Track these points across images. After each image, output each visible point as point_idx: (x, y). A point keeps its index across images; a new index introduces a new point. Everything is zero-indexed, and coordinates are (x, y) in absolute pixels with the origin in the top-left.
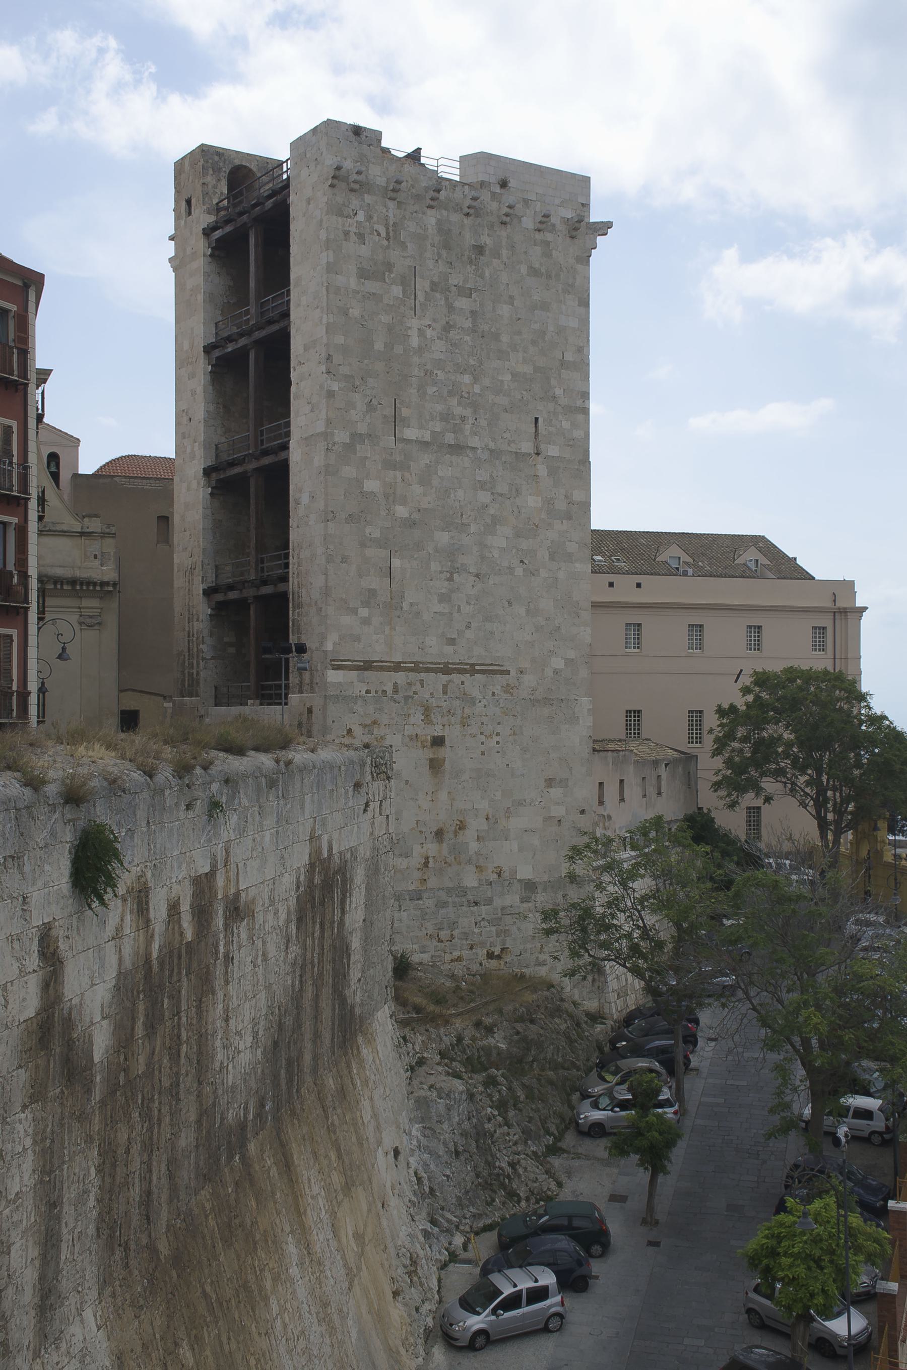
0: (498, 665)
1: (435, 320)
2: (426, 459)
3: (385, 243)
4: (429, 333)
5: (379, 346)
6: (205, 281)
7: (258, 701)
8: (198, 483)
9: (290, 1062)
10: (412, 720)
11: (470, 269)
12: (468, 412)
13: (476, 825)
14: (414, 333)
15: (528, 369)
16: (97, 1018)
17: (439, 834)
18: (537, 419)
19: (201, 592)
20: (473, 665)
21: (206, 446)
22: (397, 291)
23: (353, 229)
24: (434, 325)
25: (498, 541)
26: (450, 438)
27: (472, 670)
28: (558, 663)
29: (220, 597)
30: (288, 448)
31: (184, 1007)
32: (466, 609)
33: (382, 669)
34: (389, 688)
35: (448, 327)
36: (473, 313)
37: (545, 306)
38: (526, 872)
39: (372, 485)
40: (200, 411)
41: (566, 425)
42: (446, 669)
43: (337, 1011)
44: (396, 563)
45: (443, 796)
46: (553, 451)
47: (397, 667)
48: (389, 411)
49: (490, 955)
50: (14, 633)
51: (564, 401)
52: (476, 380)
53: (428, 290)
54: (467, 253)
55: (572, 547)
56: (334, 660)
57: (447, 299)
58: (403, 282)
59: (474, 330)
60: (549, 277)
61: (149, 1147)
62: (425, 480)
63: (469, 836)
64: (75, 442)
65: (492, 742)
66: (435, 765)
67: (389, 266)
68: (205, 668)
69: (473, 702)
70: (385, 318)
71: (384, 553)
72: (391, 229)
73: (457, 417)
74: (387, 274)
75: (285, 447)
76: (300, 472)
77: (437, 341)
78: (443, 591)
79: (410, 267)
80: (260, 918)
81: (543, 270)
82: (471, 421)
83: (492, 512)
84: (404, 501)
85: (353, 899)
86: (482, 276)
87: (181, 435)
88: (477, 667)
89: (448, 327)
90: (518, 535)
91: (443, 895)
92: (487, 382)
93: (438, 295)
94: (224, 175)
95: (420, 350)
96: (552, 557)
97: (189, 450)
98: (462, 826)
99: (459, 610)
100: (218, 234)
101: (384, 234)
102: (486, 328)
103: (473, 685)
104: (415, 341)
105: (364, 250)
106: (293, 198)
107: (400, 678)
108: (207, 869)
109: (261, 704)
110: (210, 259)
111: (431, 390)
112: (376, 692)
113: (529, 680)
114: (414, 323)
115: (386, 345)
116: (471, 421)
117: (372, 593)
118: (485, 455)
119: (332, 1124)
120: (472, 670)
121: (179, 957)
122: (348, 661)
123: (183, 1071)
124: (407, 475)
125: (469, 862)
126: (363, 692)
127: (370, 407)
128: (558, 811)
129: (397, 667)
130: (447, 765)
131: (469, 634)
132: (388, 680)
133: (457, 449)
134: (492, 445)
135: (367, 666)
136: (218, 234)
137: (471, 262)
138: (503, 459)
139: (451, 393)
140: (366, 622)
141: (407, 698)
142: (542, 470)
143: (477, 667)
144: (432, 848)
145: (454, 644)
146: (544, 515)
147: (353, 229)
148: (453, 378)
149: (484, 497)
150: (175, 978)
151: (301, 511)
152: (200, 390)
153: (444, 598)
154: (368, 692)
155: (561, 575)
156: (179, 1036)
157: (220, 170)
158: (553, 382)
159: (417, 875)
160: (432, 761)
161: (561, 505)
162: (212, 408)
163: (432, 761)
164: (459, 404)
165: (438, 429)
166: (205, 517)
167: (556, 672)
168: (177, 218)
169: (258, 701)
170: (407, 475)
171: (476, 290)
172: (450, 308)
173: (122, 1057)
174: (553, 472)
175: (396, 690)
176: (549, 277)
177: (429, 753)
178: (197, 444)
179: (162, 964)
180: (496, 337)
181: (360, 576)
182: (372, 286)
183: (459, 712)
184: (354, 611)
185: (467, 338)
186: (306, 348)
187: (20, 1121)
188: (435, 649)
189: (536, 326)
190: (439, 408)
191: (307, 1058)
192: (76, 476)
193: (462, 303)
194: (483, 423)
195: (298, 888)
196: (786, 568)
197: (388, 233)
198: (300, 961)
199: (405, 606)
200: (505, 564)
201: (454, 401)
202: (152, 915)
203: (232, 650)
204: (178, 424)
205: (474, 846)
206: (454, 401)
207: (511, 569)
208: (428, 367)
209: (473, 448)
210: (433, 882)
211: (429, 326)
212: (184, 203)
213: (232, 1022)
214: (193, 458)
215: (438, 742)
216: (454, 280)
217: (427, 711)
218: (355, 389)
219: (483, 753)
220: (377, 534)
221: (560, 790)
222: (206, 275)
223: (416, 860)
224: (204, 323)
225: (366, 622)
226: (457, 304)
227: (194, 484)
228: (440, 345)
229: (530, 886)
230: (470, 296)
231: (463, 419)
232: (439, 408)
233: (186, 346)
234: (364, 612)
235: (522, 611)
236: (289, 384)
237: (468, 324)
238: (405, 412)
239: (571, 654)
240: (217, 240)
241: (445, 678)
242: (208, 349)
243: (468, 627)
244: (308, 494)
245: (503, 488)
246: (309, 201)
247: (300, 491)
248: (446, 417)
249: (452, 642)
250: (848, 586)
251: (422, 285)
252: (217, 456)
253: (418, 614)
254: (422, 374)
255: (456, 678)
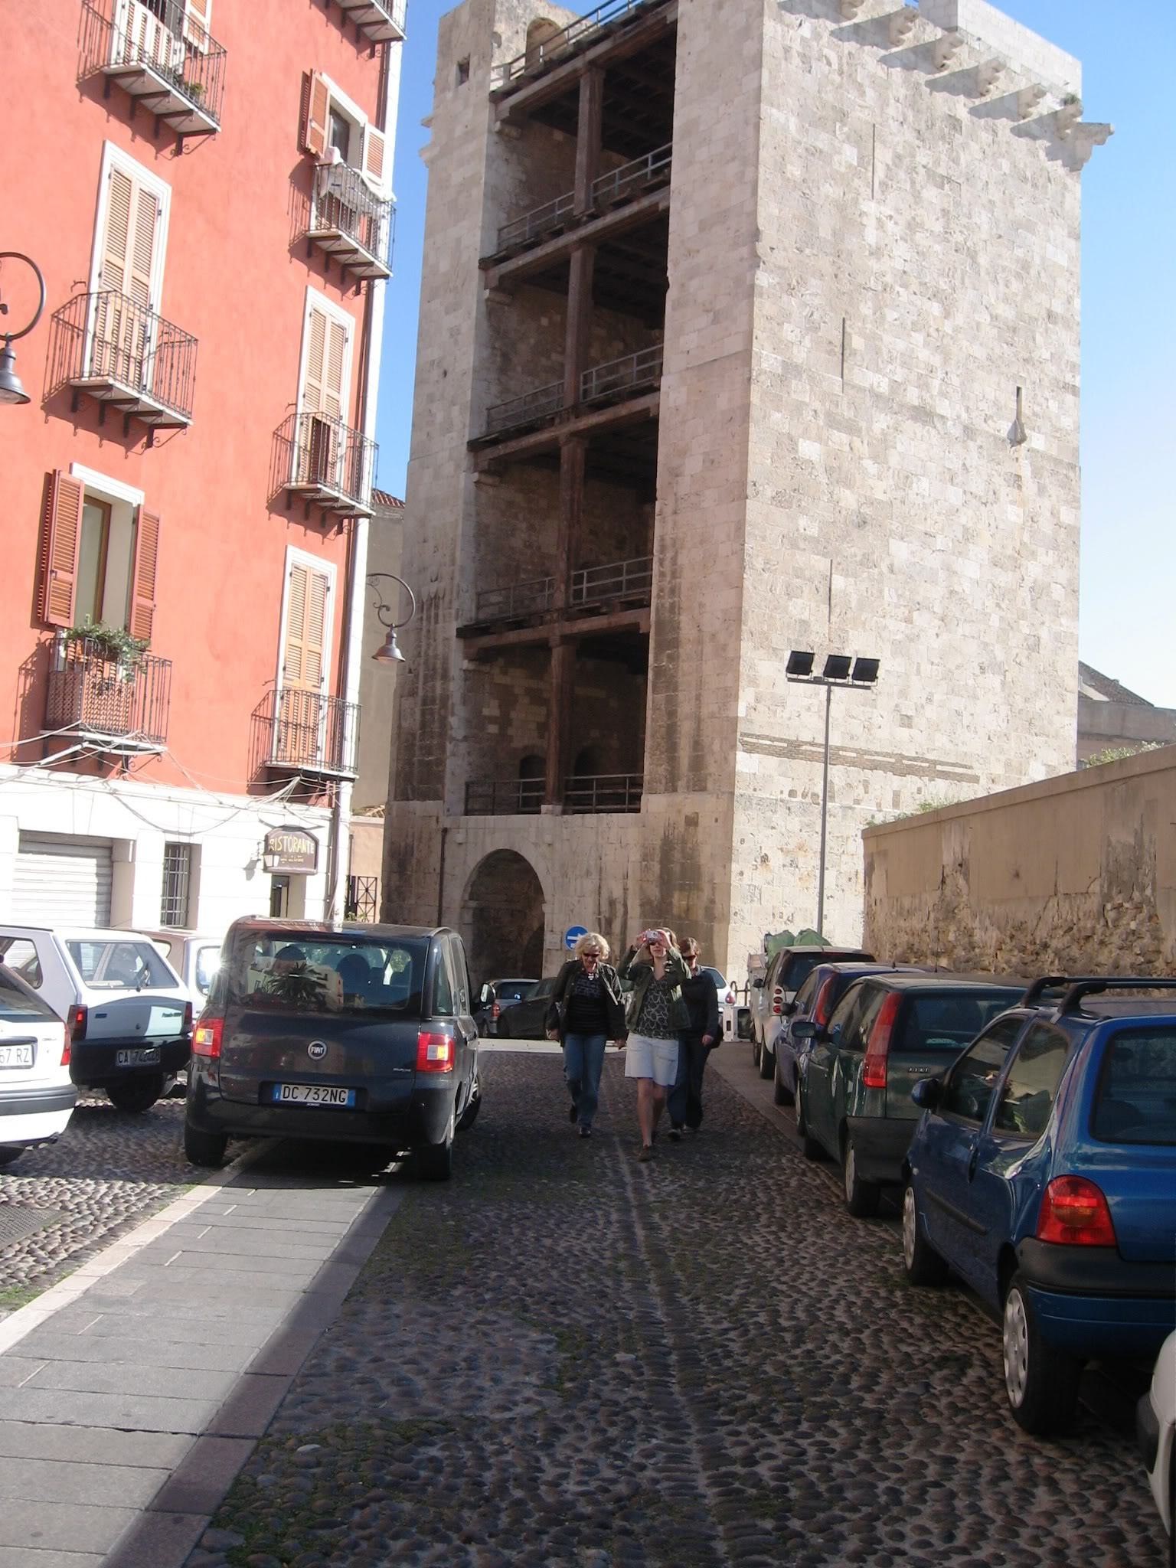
0: (965, 767)
1: (898, 210)
2: (881, 422)
3: (837, 78)
5: (825, 232)
6: (488, 167)
7: (559, 808)
8: (458, 466)
11: (943, 147)
14: (870, 223)
19: (455, 633)
20: (935, 763)
24: (896, 216)
25: (972, 568)
26: (913, 396)
29: (486, 641)
30: (658, 389)
40: (466, 354)
52: (947, 315)
53: (890, 163)
54: (938, 123)
56: (748, 735)
67: (843, 116)
68: (453, 754)
72: (844, 60)
73: (922, 366)
74: (838, 125)
76: (684, 422)
77: (901, 242)
78: (899, 637)
79: (867, 123)
83: (963, 520)
86: (956, 161)
88: (939, 768)
89: (913, 226)
94: (523, 28)
97: (440, 417)
99: (918, 672)
101: (835, 66)
104: (871, 236)
109: (564, 812)
110: (496, 138)
112: (804, 796)
114: (870, 207)
116: (940, 374)
118: (957, 432)
122: (767, 737)
124: (857, 442)
126: (785, 796)
133: (923, 414)
137: (943, 138)
138: (979, 443)
143: (939, 768)
145: (910, 726)
147: (797, 47)
148: (919, 303)
149: (954, 495)
151: (684, 486)
154: (792, 793)
157: (518, 18)
161: (1046, 526)
162: (486, 353)
164: (926, 344)
165: (898, 378)
166: (467, 516)
169: (559, 808)
170: (857, 442)
178: (457, 408)
185: (937, 248)
186: (704, 226)
197: (840, 65)
201: (919, 338)
203: (493, 729)
204: (420, 381)
206: (919, 338)
208: (889, 279)
209: (943, 417)
211: (891, 217)
214: (448, 426)
216: (923, 158)
220: (813, 531)
222: (490, 159)
224: (483, 227)
227: (449, 469)
228: (902, 250)
236: (665, 285)
237: (938, 227)
241: (896, 782)
244: (701, 458)
245: (977, 486)
247: (683, 453)
249: (907, 721)
252: (489, 424)
254: (880, 288)
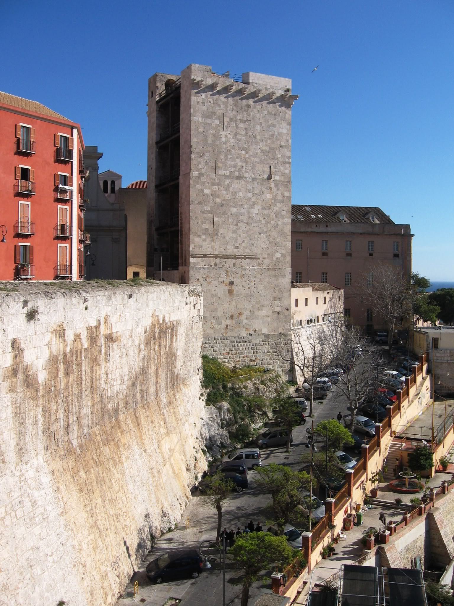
2: (227, 181)
3: (213, 105)
4: (229, 136)
6: (157, 119)
9: (142, 391)
10: (222, 276)
11: (245, 113)
12: (244, 164)
13: (247, 313)
15: (267, 148)
16: (40, 369)
17: (232, 317)
18: (270, 166)
21: (156, 178)
22: (217, 122)
23: (201, 101)
25: (255, 211)
26: (237, 174)
27: (245, 257)
28: (278, 255)
31: (83, 368)
32: (242, 235)
33: (210, 257)
34: (213, 264)
35: (236, 134)
36: (246, 129)
37: (274, 126)
38: (265, 331)
39: (206, 191)
41: (282, 168)
42: (235, 257)
43: (169, 375)
44: (216, 219)
45: (233, 303)
46: (277, 178)
47: (216, 257)
48: (214, 164)
49: (251, 360)
50: (67, 245)
51: (281, 159)
52: (247, 153)
55: (284, 213)
57: (236, 124)
58: (219, 118)
59: (246, 134)
60: (275, 115)
61: (68, 412)
62: (227, 189)
63: (243, 318)
64: (120, 177)
65: (252, 284)
66: (230, 292)
67: (214, 113)
69: (245, 269)
70: (212, 132)
71: (212, 216)
75: (178, 178)
80: (124, 341)
81: (273, 113)
82: (245, 167)
83: (253, 200)
84: (218, 197)
85: (178, 337)
86: (249, 115)
87: (149, 174)
89: (236, 134)
90: (263, 208)
91: (233, 339)
92: (251, 153)
93: (232, 123)
95: (225, 143)
96: (276, 216)
98: (240, 314)
100: (160, 103)
101: (212, 102)
102: (251, 134)
103: (246, 263)
104: (223, 139)
105: (205, 108)
106: (181, 91)
107: (217, 260)
108: (95, 324)
111: (229, 157)
113: (266, 261)
115: (212, 141)
116: (245, 167)
117: (207, 230)
119: (163, 413)
120: (245, 257)
121: (81, 352)
123: (84, 389)
124: (220, 187)
125: (243, 326)
126: (203, 266)
127: (207, 164)
128: (278, 309)
129: (216, 257)
130: (235, 292)
131: (244, 245)
132: (212, 261)
133: (240, 178)
134: (253, 176)
135: (205, 256)
136: (160, 103)
137: (245, 111)
139: (237, 158)
140: (204, 240)
141: (220, 268)
142: (272, 185)
144: (229, 322)
146: (273, 201)
149: (250, 195)
150: (79, 359)
152: (154, 158)
153: (234, 232)
154: (205, 265)
155: (280, 223)
156: (81, 378)
157: (162, 81)
158: (277, 152)
159: (223, 331)
160: (229, 290)
163: (229, 290)
167: (277, 258)
168: (149, 98)
171: (247, 120)
172: (237, 127)
173: (53, 382)
174: (276, 185)
175: (216, 265)
176: (275, 115)
177: (228, 288)
179: (72, 354)
180: (255, 137)
181: (202, 224)
182: (209, 121)
183: (240, 273)
184: (200, 236)
185: (243, 138)
186: (185, 143)
187: (5, 397)
188: (231, 250)
189: (270, 133)
190: (233, 163)
191: (152, 390)
192: (120, 188)
193: (242, 125)
194: (250, 168)
195: (145, 332)
196: (385, 220)
198: (147, 357)
199: (219, 234)
200: (258, 219)
201: (239, 160)
202: (66, 338)
205: (245, 321)
206: (239, 160)
207: (260, 221)
208: (229, 148)
210: (229, 334)
212: (151, 93)
213: (110, 376)
215: (232, 283)
217: (227, 272)
218: (201, 157)
219: (249, 288)
220: (209, 209)
221: (279, 301)
222: (157, 118)
223: (223, 326)
225: (204, 240)
226: (240, 126)
227: (152, 192)
229: (268, 336)
230: (245, 123)
231: (242, 167)
232: (233, 163)
233: (151, 142)
234: (204, 237)
235: (264, 236)
236: (180, 155)
237: (244, 133)
238: (220, 165)
239: (283, 252)
240: (161, 105)
241: (234, 261)
242: (157, 143)
243: (243, 242)
246: (186, 92)
248: (235, 166)
249: (237, 247)
250: (407, 227)
251: (227, 120)
253: (224, 237)
255: (239, 261)
